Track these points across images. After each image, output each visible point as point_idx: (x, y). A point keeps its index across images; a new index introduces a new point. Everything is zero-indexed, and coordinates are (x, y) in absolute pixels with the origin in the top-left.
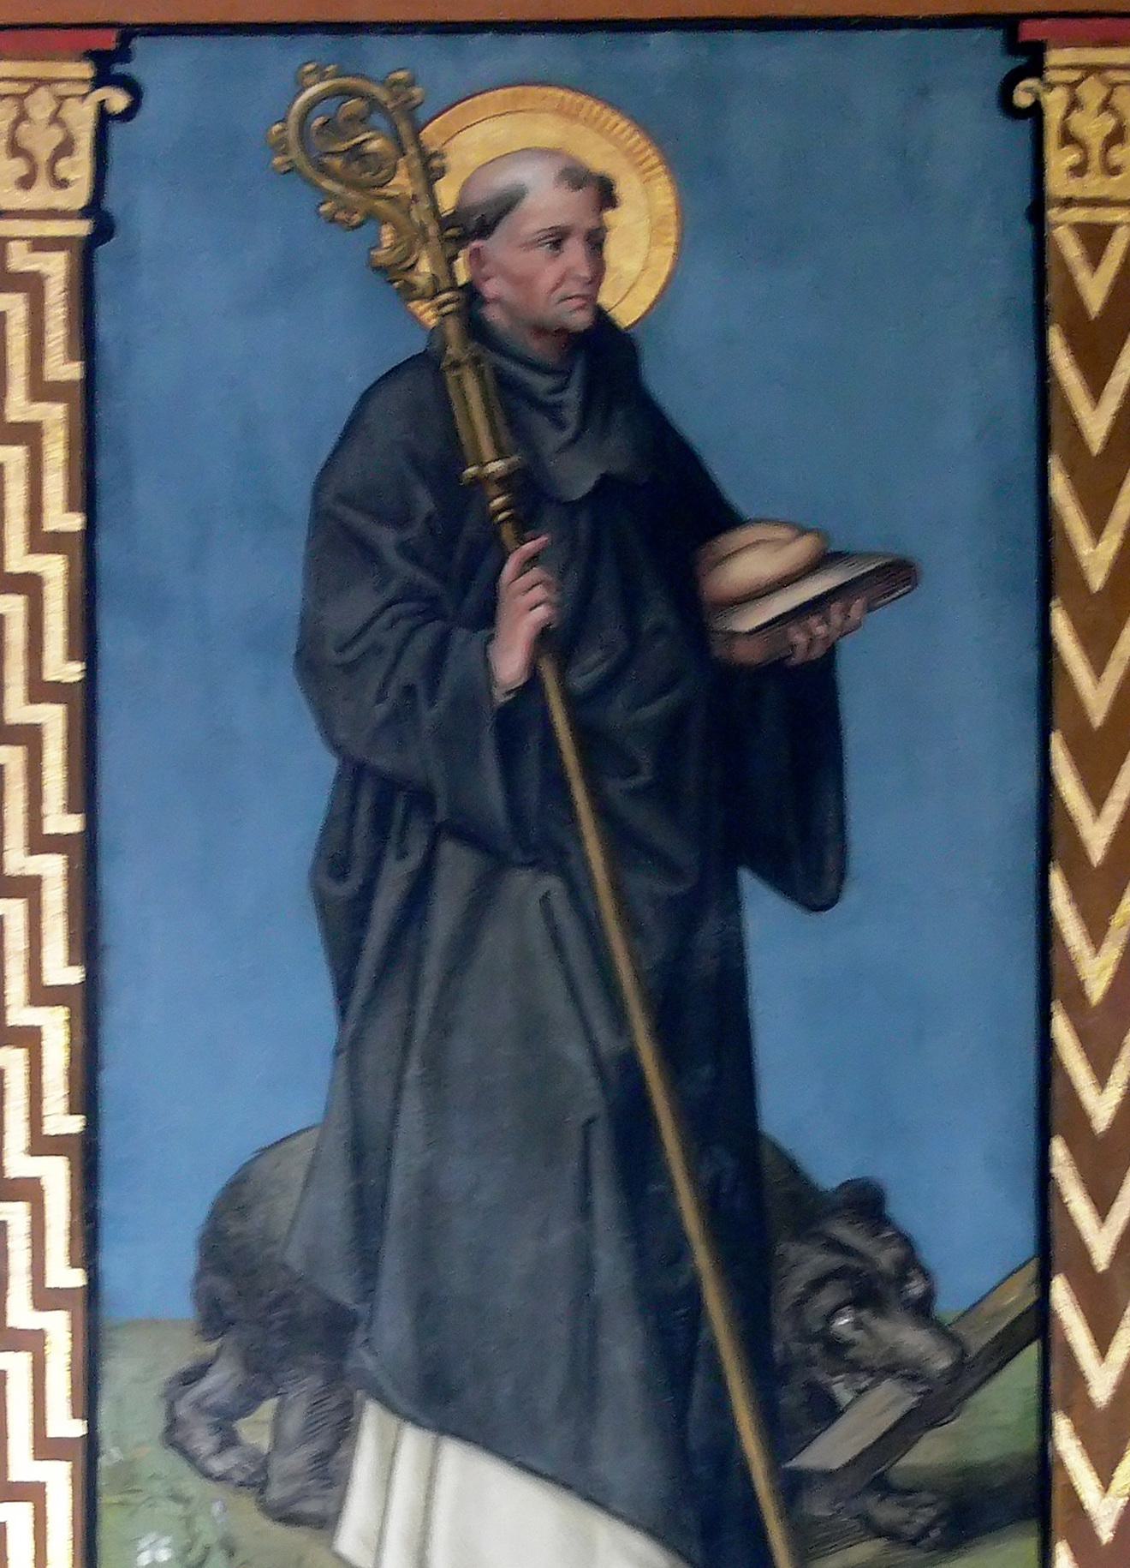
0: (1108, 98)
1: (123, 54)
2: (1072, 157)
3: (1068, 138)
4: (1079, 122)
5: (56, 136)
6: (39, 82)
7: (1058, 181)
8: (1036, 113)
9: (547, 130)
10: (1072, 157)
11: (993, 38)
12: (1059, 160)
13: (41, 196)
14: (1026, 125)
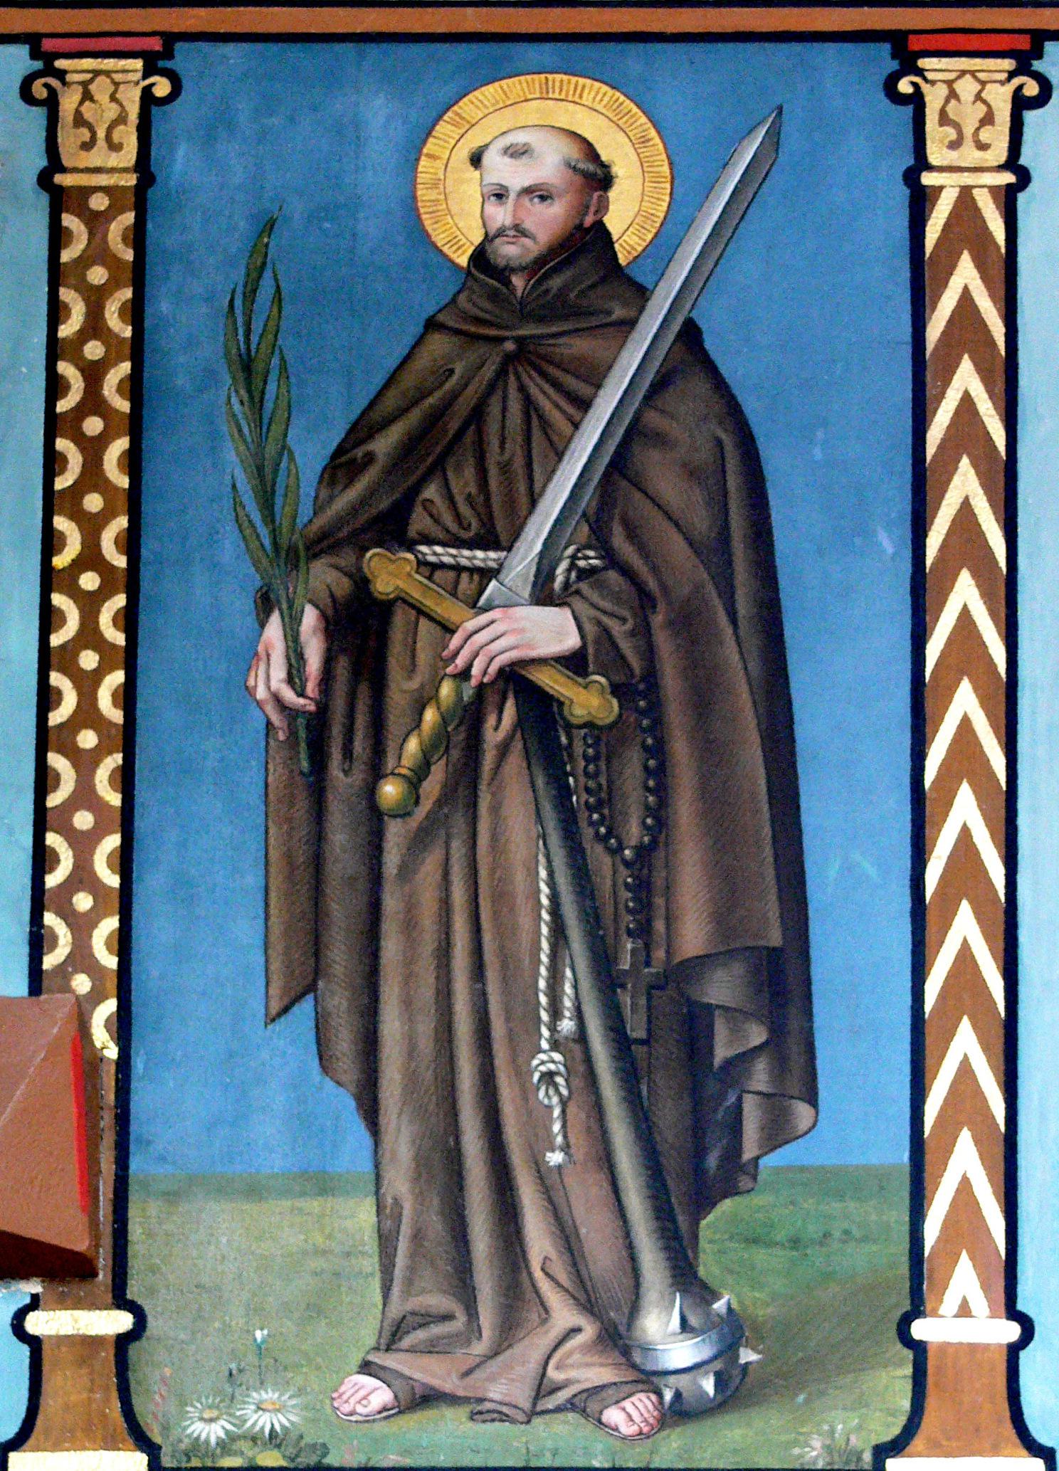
0: (980, 92)
1: (168, 53)
2: (951, 133)
3: (79, 121)
4: (88, 110)
5: (981, 110)
6: (97, 73)
7: (935, 155)
8: (917, 100)
9: (533, 112)
10: (85, 134)
11: (23, 51)
12: (69, 139)
13: (970, 155)
14: (908, 110)
